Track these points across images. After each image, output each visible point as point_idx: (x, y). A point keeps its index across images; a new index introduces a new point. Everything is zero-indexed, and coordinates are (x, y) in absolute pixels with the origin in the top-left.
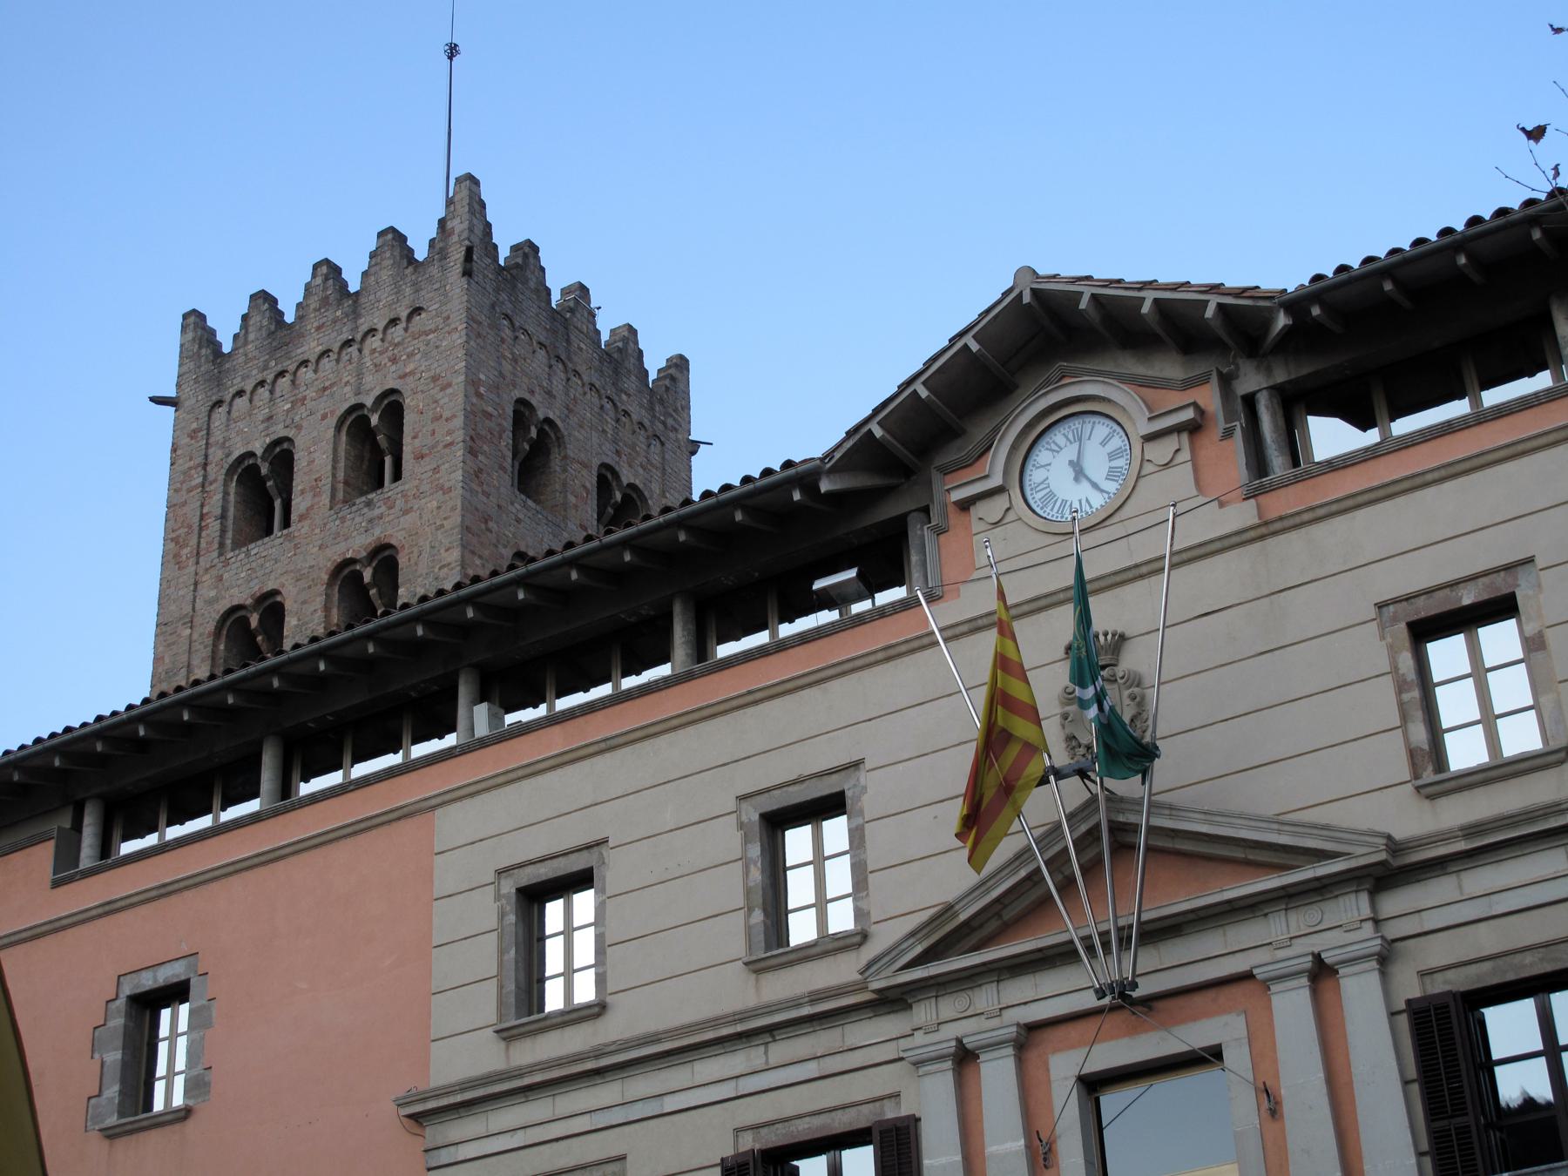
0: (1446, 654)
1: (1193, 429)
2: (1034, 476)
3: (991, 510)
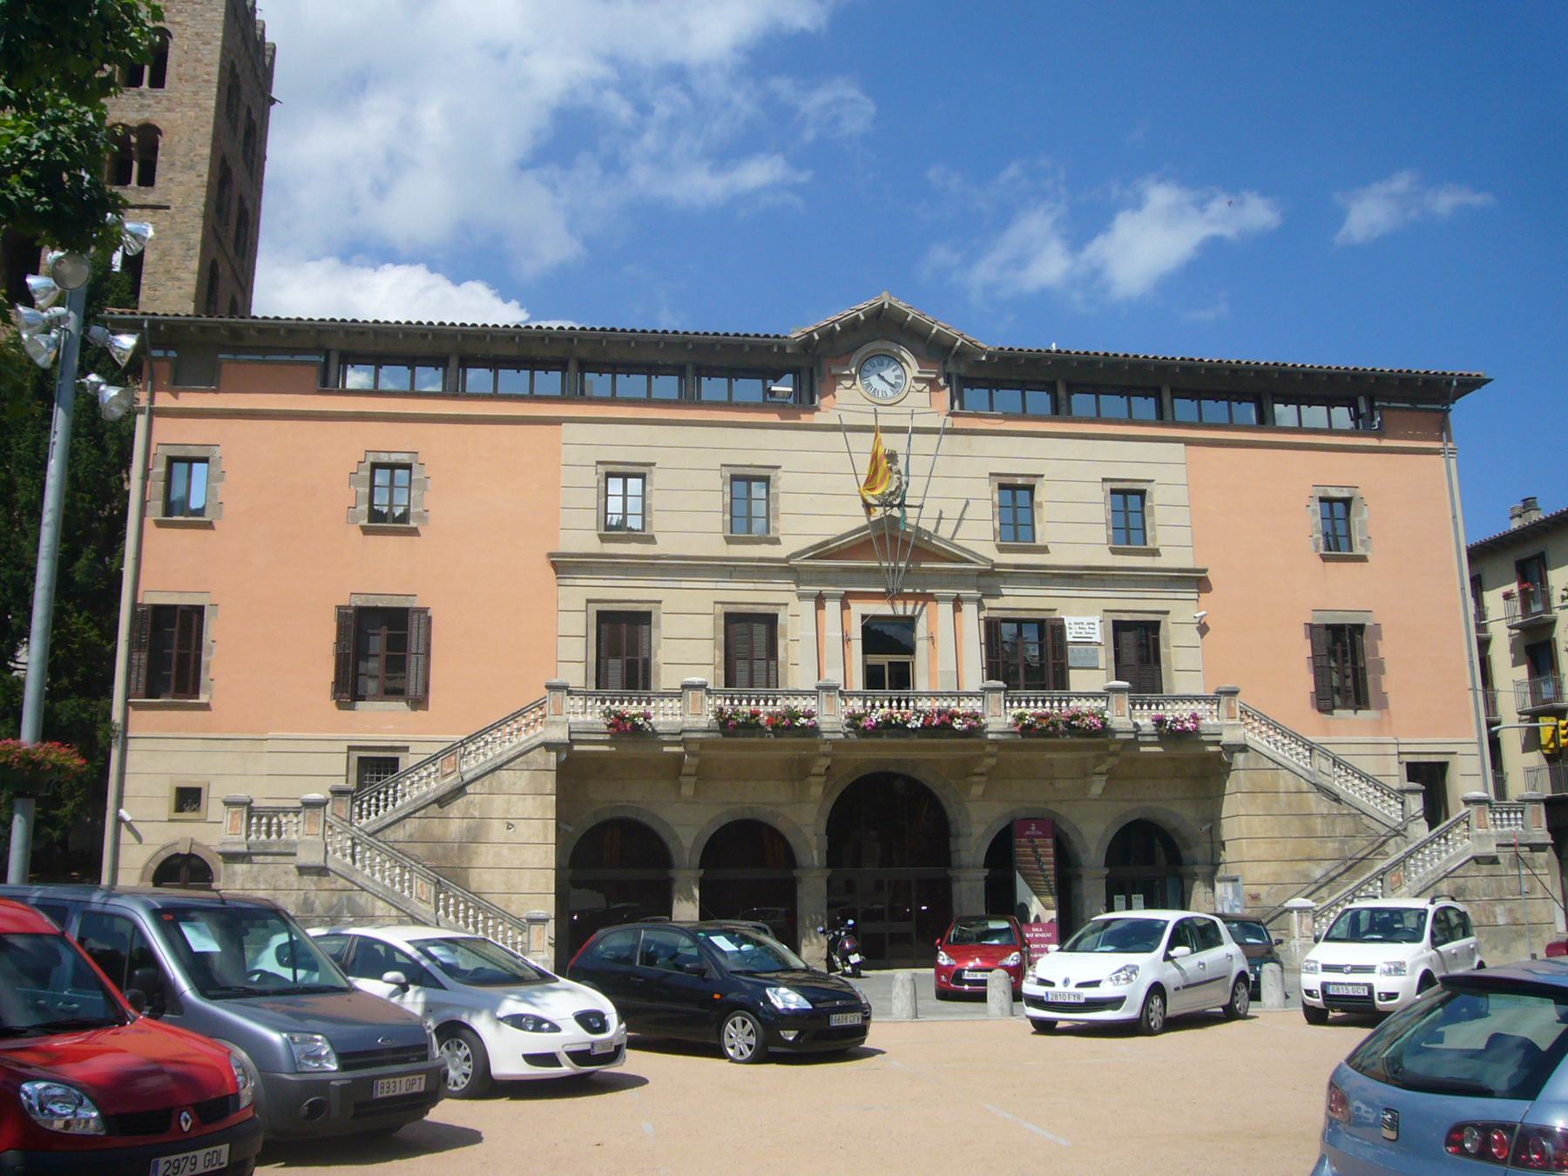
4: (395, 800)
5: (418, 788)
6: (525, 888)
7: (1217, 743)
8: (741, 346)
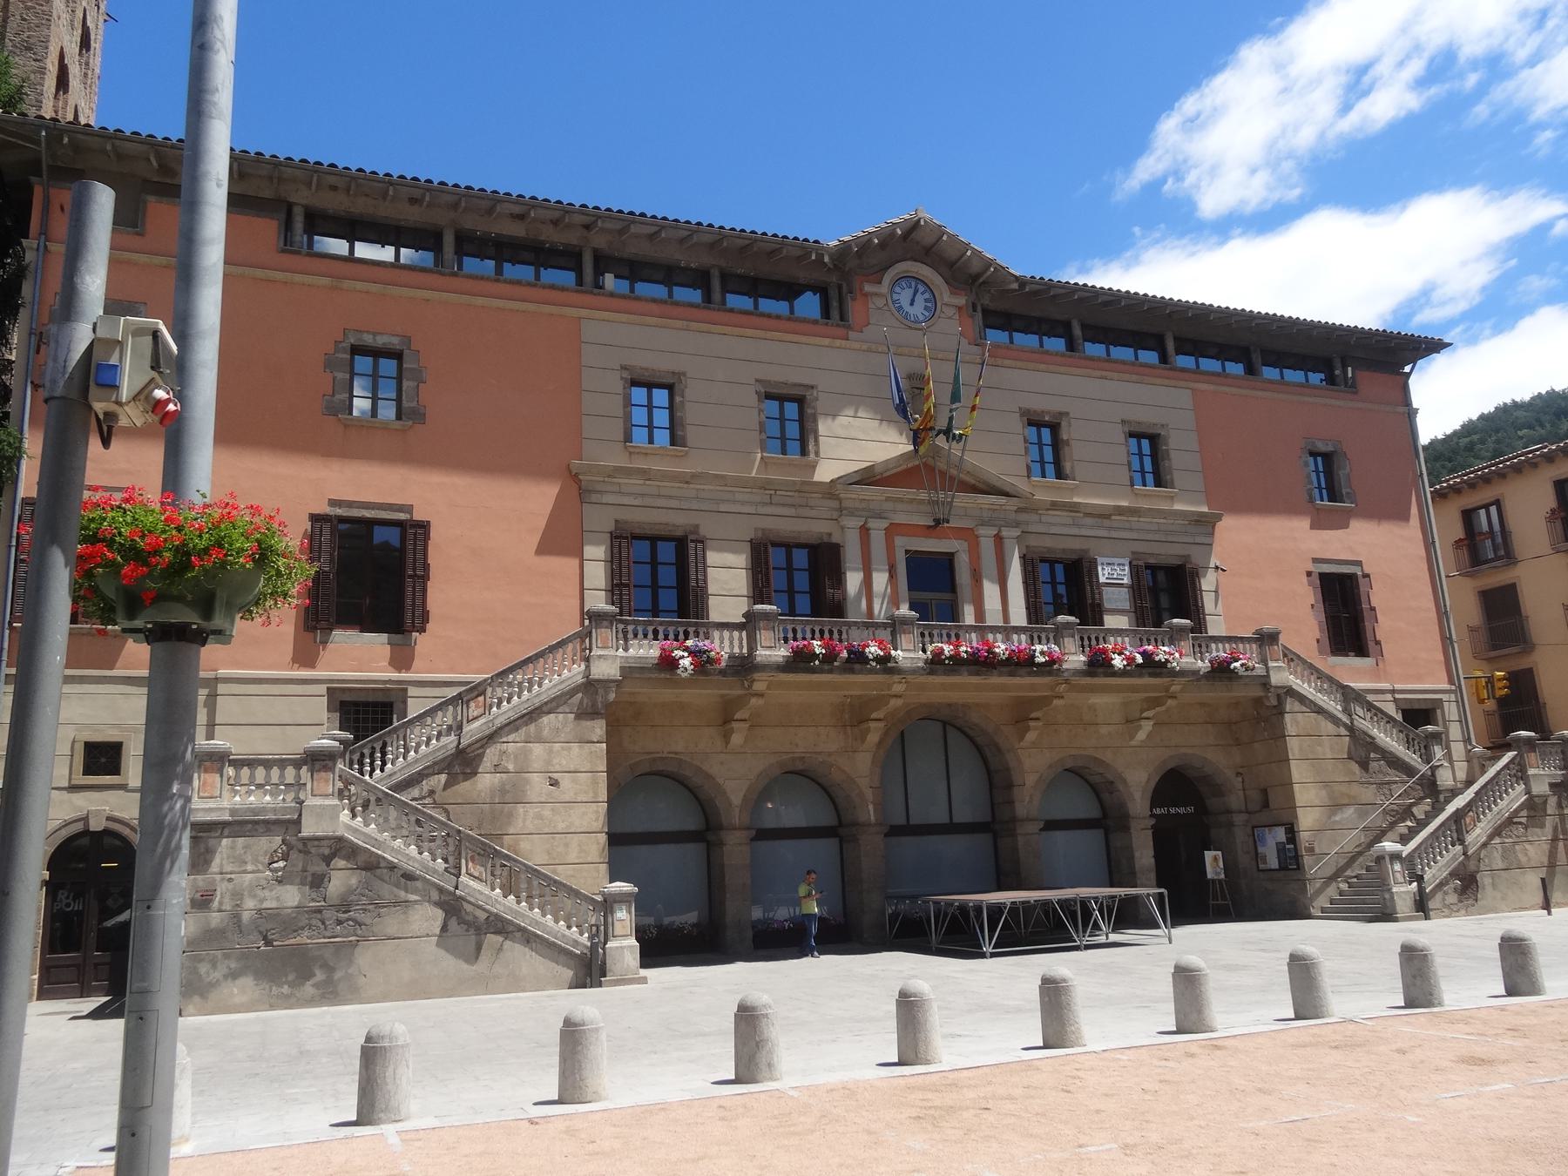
4: (384, 763)
5: (420, 746)
6: (572, 857)
8: (1119, 301)
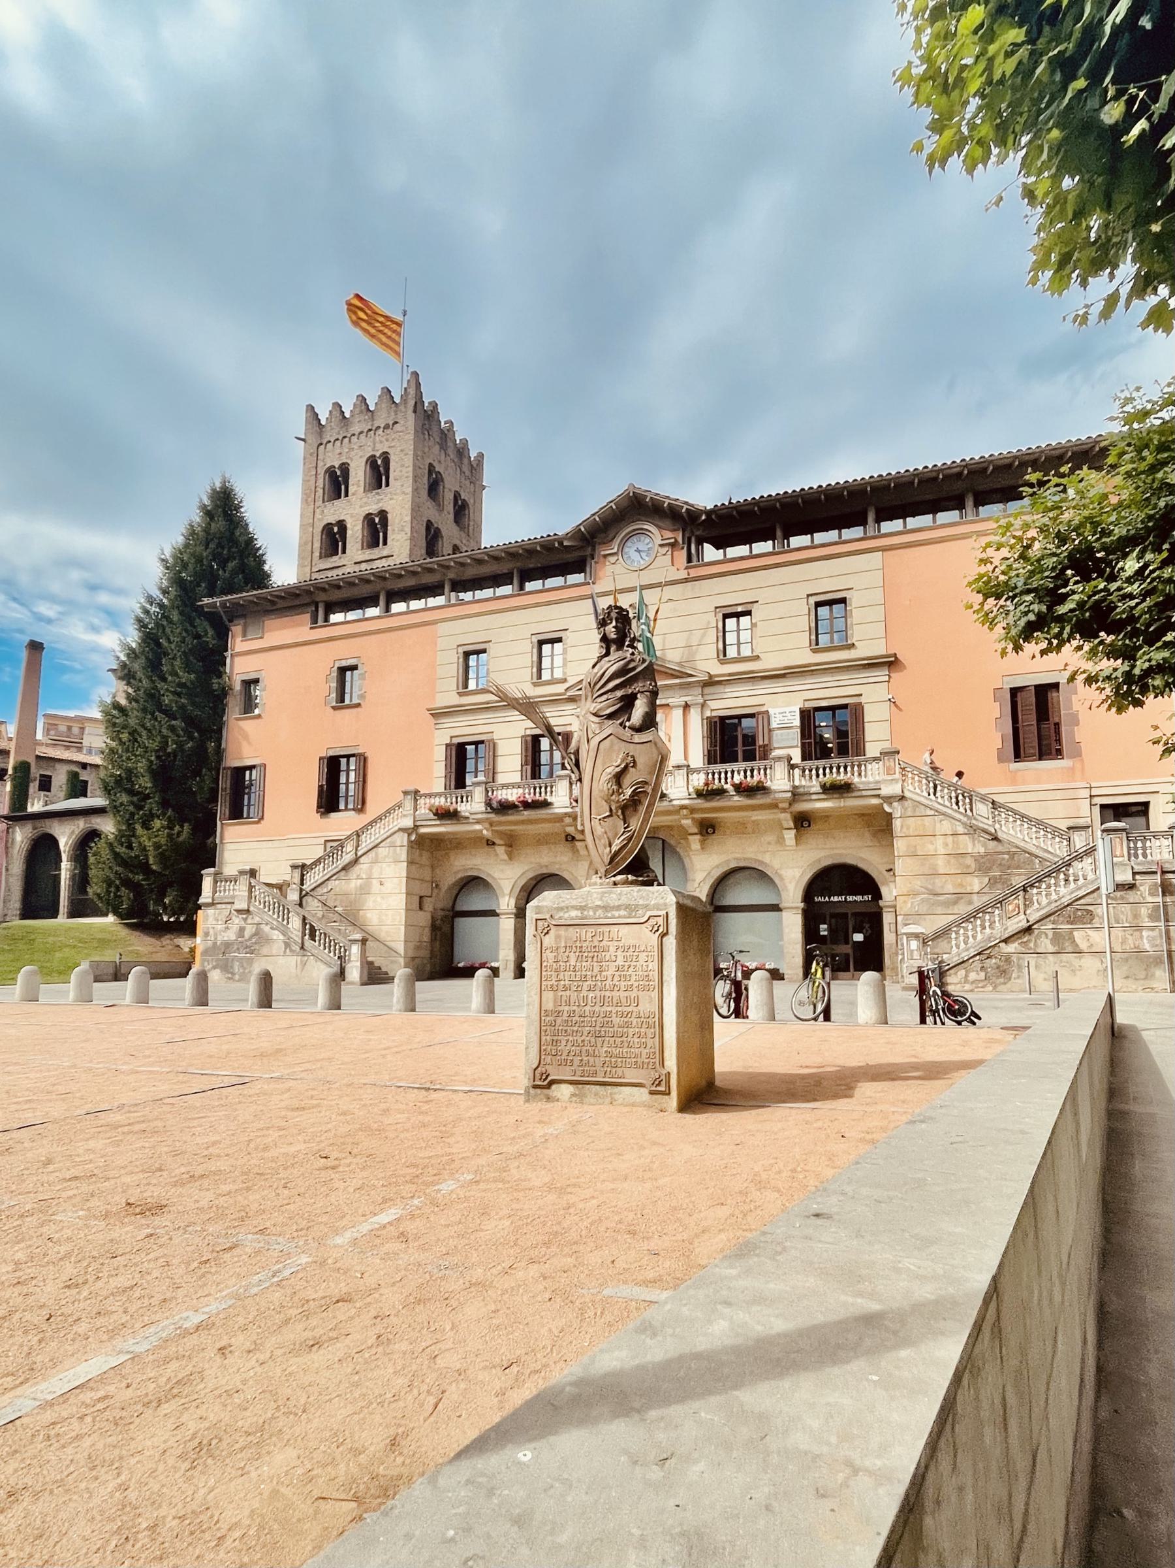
0: (731, 623)
1: (673, 545)
2: (626, 550)
3: (612, 559)
6: (389, 922)
7: (878, 796)
